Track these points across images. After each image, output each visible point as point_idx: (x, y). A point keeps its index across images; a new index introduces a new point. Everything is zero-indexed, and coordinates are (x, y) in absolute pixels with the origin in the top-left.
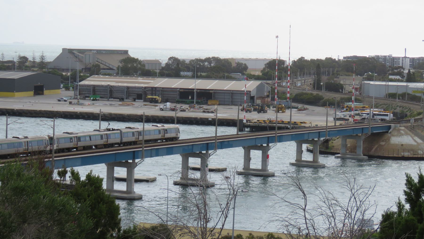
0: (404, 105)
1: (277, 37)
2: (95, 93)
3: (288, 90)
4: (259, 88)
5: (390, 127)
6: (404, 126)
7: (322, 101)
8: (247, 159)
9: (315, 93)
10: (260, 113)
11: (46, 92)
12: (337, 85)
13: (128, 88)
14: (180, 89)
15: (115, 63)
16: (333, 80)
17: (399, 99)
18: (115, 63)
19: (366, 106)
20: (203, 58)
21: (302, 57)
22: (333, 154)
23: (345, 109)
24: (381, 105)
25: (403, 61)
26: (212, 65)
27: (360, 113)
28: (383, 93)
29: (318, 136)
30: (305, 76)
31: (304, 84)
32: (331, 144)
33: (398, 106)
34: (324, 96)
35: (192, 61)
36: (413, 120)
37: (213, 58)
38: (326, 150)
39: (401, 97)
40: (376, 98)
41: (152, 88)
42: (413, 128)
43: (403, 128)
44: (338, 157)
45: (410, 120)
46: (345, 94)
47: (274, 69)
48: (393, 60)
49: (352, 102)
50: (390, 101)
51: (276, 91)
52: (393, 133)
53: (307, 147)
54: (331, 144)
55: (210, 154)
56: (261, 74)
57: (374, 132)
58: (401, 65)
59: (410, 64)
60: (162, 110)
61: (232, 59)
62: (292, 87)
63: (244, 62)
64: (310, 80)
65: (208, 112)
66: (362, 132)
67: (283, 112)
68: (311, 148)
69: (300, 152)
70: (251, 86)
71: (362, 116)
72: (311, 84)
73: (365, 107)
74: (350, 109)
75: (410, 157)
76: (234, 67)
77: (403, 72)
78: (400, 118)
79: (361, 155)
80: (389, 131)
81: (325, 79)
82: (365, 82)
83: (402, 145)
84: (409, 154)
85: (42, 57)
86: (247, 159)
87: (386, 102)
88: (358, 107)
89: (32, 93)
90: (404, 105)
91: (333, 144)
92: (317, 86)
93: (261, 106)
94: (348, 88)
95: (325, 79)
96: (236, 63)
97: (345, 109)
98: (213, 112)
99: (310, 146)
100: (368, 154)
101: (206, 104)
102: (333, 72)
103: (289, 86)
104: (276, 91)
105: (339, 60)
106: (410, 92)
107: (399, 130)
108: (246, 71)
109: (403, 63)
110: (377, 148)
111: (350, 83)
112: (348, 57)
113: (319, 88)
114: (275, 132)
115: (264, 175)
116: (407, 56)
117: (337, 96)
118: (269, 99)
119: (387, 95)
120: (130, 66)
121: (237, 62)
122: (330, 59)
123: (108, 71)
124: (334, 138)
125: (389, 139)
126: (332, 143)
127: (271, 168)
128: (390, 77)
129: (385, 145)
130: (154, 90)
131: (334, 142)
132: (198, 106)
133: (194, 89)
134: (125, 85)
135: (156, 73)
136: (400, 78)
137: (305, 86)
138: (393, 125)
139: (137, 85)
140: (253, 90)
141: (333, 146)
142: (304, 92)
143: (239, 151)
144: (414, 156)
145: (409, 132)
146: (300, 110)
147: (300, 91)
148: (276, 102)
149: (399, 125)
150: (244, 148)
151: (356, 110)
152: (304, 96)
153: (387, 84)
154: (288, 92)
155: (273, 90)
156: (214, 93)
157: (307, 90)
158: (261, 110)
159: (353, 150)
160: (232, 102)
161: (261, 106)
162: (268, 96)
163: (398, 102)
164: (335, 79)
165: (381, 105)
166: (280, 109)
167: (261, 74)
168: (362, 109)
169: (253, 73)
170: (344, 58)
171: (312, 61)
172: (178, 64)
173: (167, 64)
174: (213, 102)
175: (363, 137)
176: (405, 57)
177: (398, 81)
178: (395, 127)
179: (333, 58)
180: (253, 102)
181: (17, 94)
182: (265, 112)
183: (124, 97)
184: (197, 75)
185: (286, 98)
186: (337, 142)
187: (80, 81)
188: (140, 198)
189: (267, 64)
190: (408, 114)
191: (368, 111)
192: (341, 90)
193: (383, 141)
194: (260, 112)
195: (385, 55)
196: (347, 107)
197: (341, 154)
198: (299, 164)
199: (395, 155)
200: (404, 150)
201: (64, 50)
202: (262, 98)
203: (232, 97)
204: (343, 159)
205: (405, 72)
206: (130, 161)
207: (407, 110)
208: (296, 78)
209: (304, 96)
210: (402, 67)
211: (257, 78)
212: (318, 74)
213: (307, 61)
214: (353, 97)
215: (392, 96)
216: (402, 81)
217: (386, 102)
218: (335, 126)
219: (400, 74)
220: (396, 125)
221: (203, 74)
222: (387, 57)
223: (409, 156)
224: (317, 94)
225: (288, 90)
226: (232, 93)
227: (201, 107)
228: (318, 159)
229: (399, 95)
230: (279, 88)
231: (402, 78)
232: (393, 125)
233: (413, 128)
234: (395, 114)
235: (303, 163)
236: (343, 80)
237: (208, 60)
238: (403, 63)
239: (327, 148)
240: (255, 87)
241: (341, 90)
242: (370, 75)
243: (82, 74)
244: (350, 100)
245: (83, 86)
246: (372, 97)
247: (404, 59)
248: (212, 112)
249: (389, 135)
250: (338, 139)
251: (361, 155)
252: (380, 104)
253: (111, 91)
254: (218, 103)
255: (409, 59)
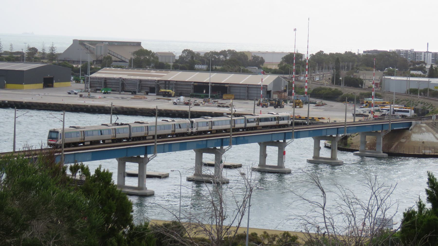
0: (426, 101)
1: (295, 30)
2: (107, 86)
3: (306, 84)
4: (276, 83)
5: (410, 124)
6: (426, 123)
7: (340, 96)
8: (263, 155)
9: (334, 88)
10: (277, 109)
11: (55, 84)
12: (357, 80)
13: (141, 81)
14: (213, 83)
15: (128, 55)
16: (353, 75)
17: (420, 95)
18: (128, 55)
19: (387, 102)
20: (218, 50)
21: (321, 51)
22: (352, 151)
23: (364, 105)
24: (402, 101)
25: (425, 55)
26: (228, 58)
27: (380, 109)
28: (404, 89)
29: (283, 138)
30: (324, 70)
31: (323, 79)
32: (350, 141)
33: (419, 102)
34: (343, 92)
35: (207, 54)
36: (435, 117)
37: (229, 51)
38: (344, 146)
39: (422, 93)
40: (397, 94)
41: (166, 81)
42: (435, 125)
43: (424, 125)
44: (357, 155)
45: (431, 117)
46: (365, 89)
47: (292, 63)
48: (415, 54)
49: (372, 97)
50: (411, 97)
51: (293, 86)
52: (414, 130)
53: (325, 144)
54: (350, 141)
55: (224, 150)
56: (278, 68)
57: (395, 129)
58: (423, 60)
59: (432, 60)
60: (175, 104)
61: (249, 52)
62: (310, 82)
63: (260, 56)
64: (329, 74)
65: (223, 107)
66: (382, 129)
67: (301, 107)
68: (329, 144)
69: (317, 148)
70: (268, 80)
71: (382, 112)
72: (329, 79)
73: (385, 103)
74: (370, 105)
75: (432, 155)
76: (250, 60)
77: (425, 67)
78: (421, 114)
79: (380, 153)
80: (410, 128)
81: (344, 73)
82: (386, 77)
83: (423, 142)
84: (430, 151)
85: (52, 49)
86: (263, 155)
87: (407, 98)
88: (379, 103)
89: (41, 85)
90: (426, 101)
91: (352, 141)
92: (336, 81)
93: (278, 101)
94: (368, 83)
95: (344, 73)
96: (252, 56)
97: (364, 105)
98: (228, 107)
99: (328, 142)
100: (387, 152)
101: (221, 98)
102: (352, 66)
103: (306, 81)
104: (293, 86)
105: (359, 54)
106: (432, 88)
107: (420, 127)
108: (263, 65)
109: (425, 58)
110: (397, 145)
111: (370, 78)
112: (368, 52)
113: (338, 82)
114: (292, 128)
115: (280, 172)
116: (429, 51)
117: (356, 92)
118: (286, 94)
119: (408, 90)
120: (143, 58)
121: (253, 55)
122: (350, 53)
123: (120, 64)
124: (353, 135)
125: (409, 136)
126: (351, 139)
127: (288, 165)
128: (412, 72)
129: (405, 142)
130: (167, 84)
131: (352, 138)
132: (213, 100)
133: (208, 83)
134: (138, 78)
135: (169, 66)
136: (422, 74)
137: (324, 81)
138: (413, 122)
139: (150, 78)
140: (270, 85)
141: (352, 143)
142: (322, 86)
143: (255, 147)
144: (436, 154)
145: (430, 129)
146: (318, 106)
147: (318, 86)
148: (293, 97)
149: (420, 122)
150: (260, 144)
151: (376, 106)
152: (323, 91)
153: (408, 79)
154: (306, 87)
155: (290, 84)
156: (230, 87)
157: (325, 84)
158: (278, 105)
159: (373, 147)
160: (248, 96)
161: (278, 101)
162: (285, 91)
163: (419, 98)
164: (355, 74)
165: (402, 101)
166: (297, 104)
167: (278, 68)
168: (382, 105)
169: (269, 67)
170: (364, 52)
171: (331, 55)
172: (192, 57)
173: (181, 57)
174: (228, 96)
175: (383, 134)
176: (428, 52)
177: (420, 76)
178: (417, 124)
179: (353, 52)
180: (270, 97)
181: (26, 86)
182: (282, 107)
183: (137, 90)
184: (212, 68)
185: (303, 93)
186: (355, 139)
187: (90, 74)
188: (152, 195)
189: (285, 58)
190: (430, 110)
191: (388, 107)
192: (360, 85)
193: (403, 138)
194: (277, 107)
195: (407, 49)
196: (367, 102)
197: (360, 151)
198: (316, 161)
199: (416, 153)
200: (425, 148)
201: (75, 41)
202: (279, 92)
203: (248, 92)
204: (362, 156)
205: (427, 67)
206: (142, 156)
207: (429, 106)
208: (314, 73)
209: (323, 91)
210: (424, 62)
211: (274, 72)
212: (337, 69)
213: (325, 55)
214: (373, 93)
215: (414, 92)
216: (424, 77)
217: (407, 98)
218: (354, 122)
219: (422, 69)
220: (417, 121)
221: (218, 67)
222: (409, 52)
223: (430, 154)
224: (336, 89)
225: (306, 84)
226: (248, 87)
227: (216, 102)
228: (336, 156)
229: (421, 91)
230: (297, 83)
231: (424, 73)
232: (413, 122)
233: (435, 125)
234: (416, 110)
235: (321, 160)
236: (362, 75)
237: (223, 53)
238: (425, 58)
239: (346, 144)
240: (272, 81)
241: (360, 85)
242: (389, 70)
243: (93, 67)
244: (369, 95)
245: (94, 78)
246: (392, 93)
247: (426, 54)
248: (227, 107)
249: (410, 132)
250: (357, 135)
251: (380, 153)
252: (401, 100)
253: (123, 84)
254: (233, 98)
255: (431, 54)
